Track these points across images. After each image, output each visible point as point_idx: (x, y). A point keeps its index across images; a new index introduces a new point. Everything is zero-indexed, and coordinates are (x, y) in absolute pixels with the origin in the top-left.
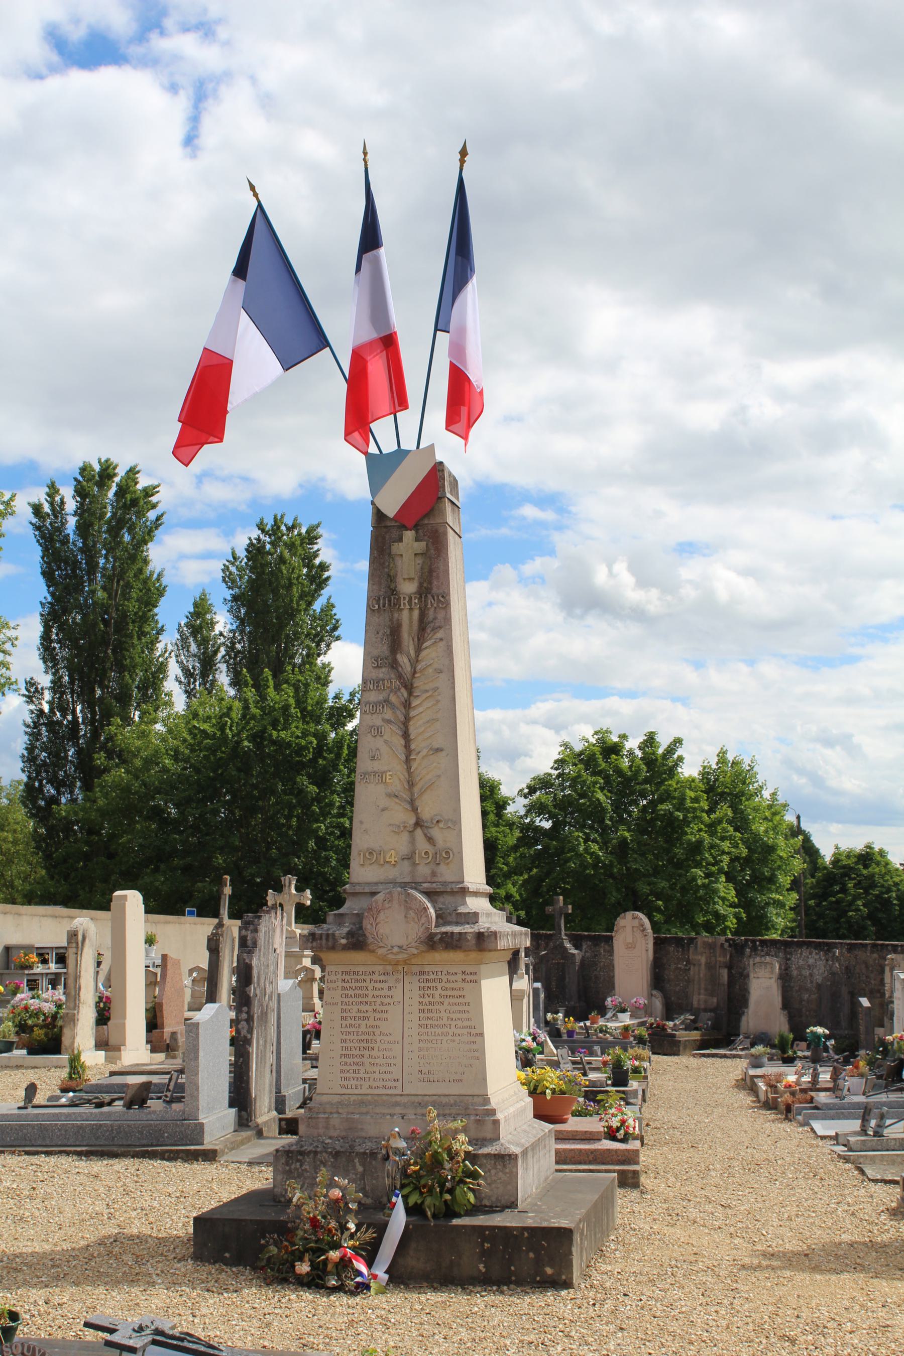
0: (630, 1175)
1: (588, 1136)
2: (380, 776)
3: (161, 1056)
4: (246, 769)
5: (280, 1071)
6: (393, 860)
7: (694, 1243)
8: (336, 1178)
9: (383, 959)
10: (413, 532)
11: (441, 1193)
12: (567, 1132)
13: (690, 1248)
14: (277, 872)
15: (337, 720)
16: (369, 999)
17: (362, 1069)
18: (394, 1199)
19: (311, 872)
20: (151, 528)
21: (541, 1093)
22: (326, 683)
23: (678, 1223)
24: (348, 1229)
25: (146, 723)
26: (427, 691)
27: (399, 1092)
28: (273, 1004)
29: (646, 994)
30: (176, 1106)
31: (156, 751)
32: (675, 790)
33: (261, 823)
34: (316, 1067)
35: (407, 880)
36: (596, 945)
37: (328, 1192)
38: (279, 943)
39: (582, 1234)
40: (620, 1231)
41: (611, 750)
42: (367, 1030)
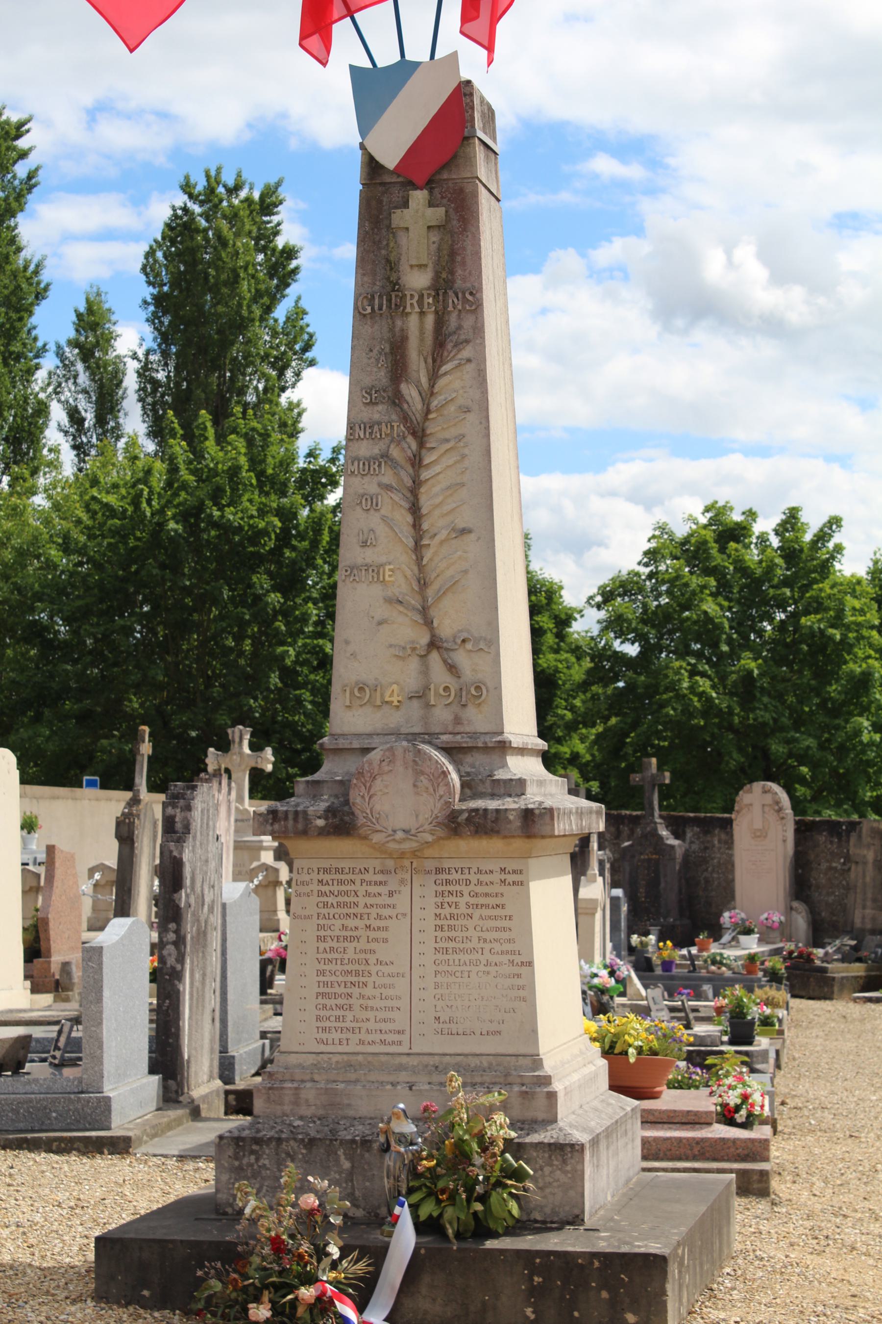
0: (755, 1177)
1: (691, 1118)
2: (375, 570)
3: (46, 999)
4: (173, 566)
5: (227, 1020)
6: (395, 699)
7: (852, 1280)
8: (311, 1179)
9: (381, 850)
10: (425, 192)
11: (469, 1200)
12: (661, 1112)
13: (845, 1288)
14: (222, 718)
15: (313, 490)
16: (360, 910)
17: (349, 1016)
18: (397, 1210)
19: (274, 722)
20: (21, 190)
21: (621, 1054)
22: (294, 433)
23: (827, 1250)
24: (328, 1254)
25: (19, 494)
26: (447, 441)
27: (404, 1049)
28: (216, 920)
29: (782, 906)
30: (67, 1072)
31: (36, 538)
32: (829, 597)
33: (197, 647)
34: (280, 1014)
35: (416, 730)
36: (706, 832)
37: (297, 1198)
38: (225, 827)
39: (681, 1264)
40: (740, 1261)
41: (730, 533)
42: (356, 957)
